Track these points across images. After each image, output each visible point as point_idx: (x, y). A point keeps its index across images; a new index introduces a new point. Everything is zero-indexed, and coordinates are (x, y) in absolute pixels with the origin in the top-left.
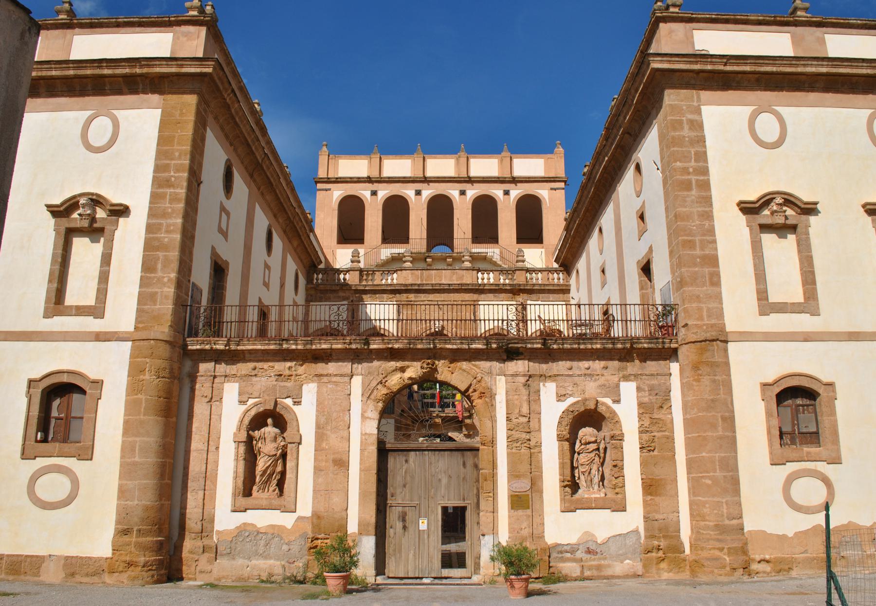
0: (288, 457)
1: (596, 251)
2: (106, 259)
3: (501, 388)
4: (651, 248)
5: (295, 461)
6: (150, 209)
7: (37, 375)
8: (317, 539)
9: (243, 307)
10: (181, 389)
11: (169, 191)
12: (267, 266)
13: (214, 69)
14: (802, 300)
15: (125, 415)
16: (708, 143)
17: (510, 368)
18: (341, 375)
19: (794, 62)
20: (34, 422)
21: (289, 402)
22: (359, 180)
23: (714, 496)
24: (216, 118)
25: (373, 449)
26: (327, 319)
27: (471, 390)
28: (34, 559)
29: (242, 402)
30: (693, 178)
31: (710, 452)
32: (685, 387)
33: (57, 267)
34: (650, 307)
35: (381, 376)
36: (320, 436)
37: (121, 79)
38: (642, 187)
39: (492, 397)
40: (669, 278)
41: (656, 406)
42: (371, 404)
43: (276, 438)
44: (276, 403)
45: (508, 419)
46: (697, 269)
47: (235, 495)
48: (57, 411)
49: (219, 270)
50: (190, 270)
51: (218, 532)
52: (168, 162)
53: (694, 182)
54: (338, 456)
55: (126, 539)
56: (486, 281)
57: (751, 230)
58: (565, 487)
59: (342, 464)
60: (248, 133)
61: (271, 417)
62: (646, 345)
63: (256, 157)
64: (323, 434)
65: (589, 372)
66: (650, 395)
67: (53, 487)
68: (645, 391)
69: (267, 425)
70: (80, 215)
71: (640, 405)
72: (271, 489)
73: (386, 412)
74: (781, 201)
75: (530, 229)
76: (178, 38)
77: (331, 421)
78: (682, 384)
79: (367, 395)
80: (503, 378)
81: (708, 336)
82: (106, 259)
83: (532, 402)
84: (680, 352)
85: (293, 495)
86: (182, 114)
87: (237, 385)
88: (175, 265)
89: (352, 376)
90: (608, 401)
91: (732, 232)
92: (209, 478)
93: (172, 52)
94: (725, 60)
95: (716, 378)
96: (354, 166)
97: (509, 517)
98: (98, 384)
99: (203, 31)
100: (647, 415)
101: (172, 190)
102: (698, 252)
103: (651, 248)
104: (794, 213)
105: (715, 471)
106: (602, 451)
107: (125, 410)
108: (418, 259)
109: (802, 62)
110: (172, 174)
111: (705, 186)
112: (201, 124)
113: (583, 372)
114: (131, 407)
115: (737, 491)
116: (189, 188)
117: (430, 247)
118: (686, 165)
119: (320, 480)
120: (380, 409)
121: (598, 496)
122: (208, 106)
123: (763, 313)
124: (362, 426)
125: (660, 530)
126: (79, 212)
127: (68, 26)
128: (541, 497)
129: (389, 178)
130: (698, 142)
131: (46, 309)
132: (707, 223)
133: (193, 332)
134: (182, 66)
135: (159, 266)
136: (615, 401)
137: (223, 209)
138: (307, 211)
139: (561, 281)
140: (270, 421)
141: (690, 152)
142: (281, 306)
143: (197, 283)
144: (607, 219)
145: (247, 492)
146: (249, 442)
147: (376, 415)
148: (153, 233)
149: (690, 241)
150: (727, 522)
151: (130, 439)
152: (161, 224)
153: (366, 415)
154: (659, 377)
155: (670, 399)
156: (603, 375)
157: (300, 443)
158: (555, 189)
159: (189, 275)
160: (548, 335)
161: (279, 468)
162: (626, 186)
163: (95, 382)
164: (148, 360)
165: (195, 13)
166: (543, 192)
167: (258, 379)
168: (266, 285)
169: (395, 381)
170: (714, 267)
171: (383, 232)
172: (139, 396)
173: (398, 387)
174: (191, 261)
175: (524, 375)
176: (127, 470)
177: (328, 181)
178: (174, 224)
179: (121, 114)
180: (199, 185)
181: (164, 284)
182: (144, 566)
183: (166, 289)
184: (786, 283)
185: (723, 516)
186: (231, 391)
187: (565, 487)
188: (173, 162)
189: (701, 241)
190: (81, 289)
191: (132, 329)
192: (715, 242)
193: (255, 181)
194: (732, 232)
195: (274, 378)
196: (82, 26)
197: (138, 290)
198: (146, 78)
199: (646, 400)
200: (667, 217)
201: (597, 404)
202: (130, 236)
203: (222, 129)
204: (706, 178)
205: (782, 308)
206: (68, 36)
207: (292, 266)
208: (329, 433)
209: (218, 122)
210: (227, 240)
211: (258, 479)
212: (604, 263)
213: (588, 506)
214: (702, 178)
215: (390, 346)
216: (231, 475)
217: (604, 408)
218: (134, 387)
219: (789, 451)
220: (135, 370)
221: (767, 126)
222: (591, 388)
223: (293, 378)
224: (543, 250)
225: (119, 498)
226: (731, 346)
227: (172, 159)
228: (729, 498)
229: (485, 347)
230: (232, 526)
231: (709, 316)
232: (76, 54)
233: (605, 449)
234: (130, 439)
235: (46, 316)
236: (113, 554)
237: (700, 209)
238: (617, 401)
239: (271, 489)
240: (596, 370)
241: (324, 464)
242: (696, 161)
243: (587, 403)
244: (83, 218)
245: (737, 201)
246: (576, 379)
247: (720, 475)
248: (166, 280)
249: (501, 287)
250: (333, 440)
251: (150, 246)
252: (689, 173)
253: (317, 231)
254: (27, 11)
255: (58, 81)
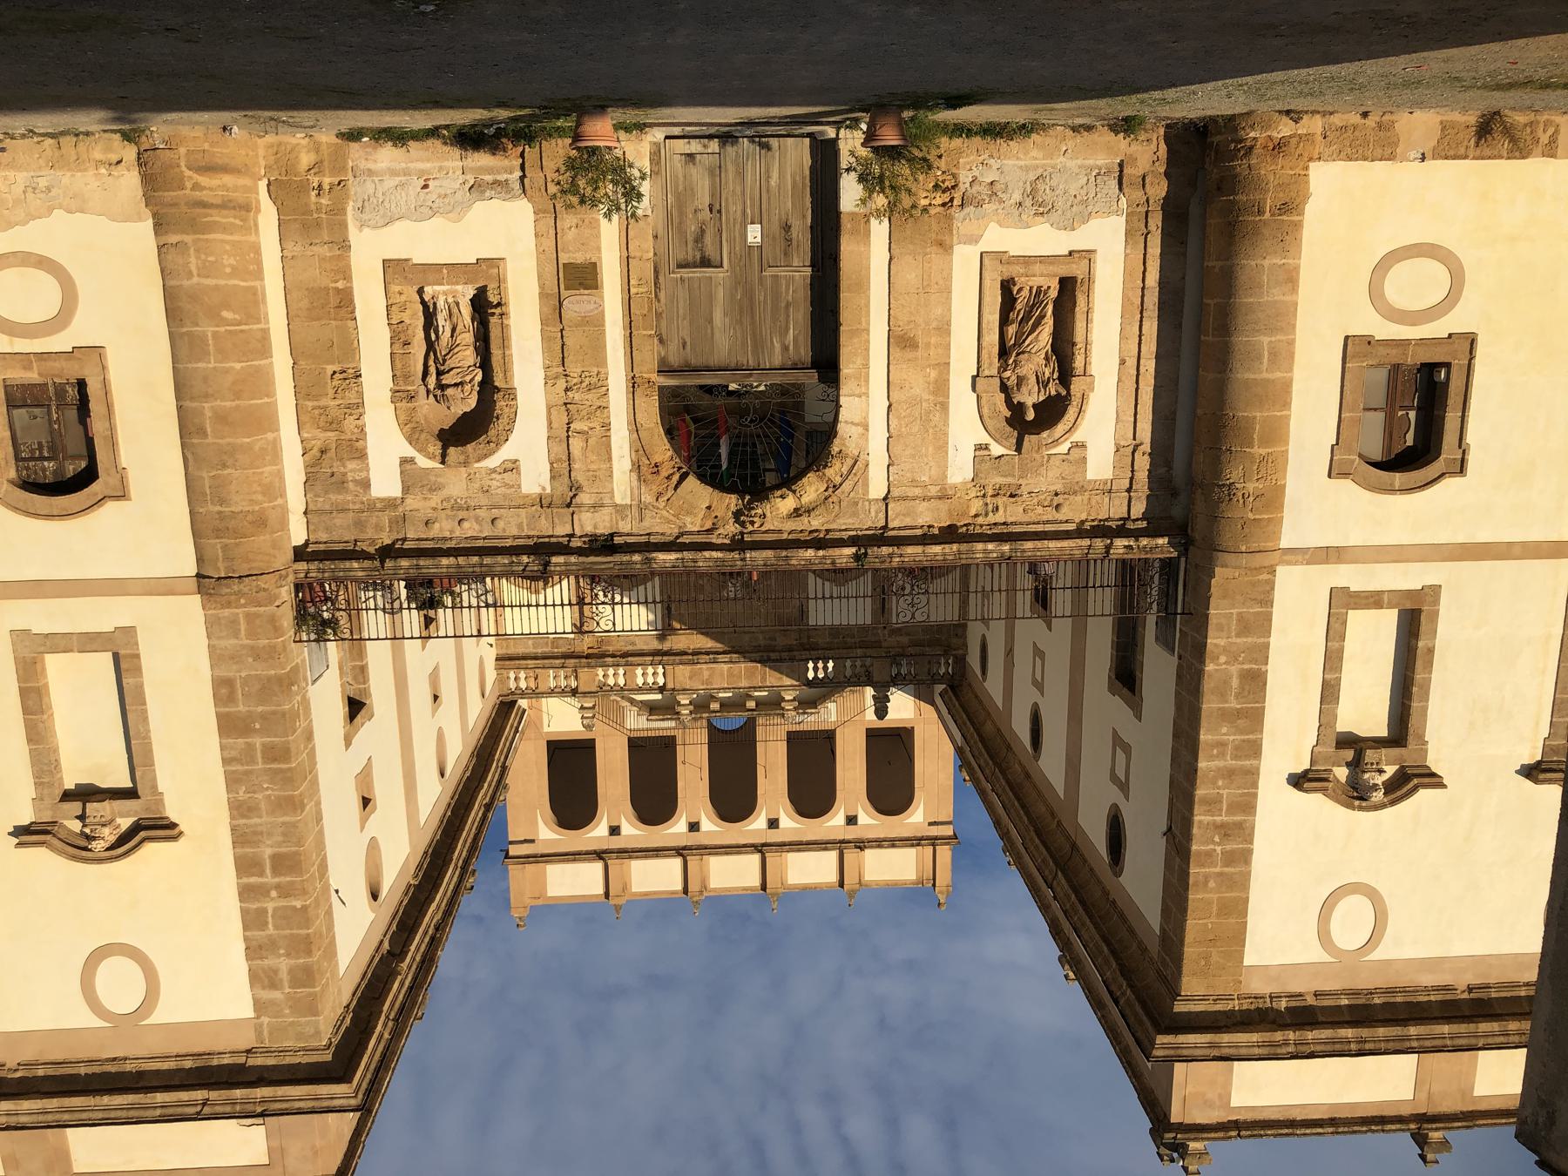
0: (996, 350)
1: (453, 731)
2: (1330, 693)
3: (622, 482)
4: (348, 742)
5: (984, 344)
6: (1255, 785)
7: (1449, 483)
8: (944, 205)
9: (1080, 616)
10: (1190, 464)
11: (1223, 818)
12: (1039, 686)
13: (1153, 1043)
14: (49, 658)
15: (1288, 417)
16: (241, 946)
17: (607, 518)
18: (905, 498)
19: (66, 1117)
20: (1454, 398)
21: (997, 450)
22: (879, 843)
23: (217, 288)
24: (1144, 950)
25: (846, 370)
26: (933, 597)
27: (676, 477)
28: (1452, 153)
29: (1082, 446)
30: (269, 879)
31: (227, 371)
32: (275, 490)
33: (1418, 677)
34: (347, 636)
35: (834, 498)
36: (941, 388)
37: (1321, 1019)
38: (367, 848)
39: (637, 467)
40: (313, 691)
41: (332, 453)
42: (852, 450)
43: (1019, 385)
44: (1019, 449)
45: (606, 426)
46: (260, 709)
47: (1090, 279)
48: (1416, 416)
49: (1126, 677)
50: (1179, 676)
51: (1117, 213)
52: (1226, 870)
53: (268, 871)
54: (910, 354)
55: (1282, 197)
56: (650, 670)
57: (155, 787)
58: (499, 304)
59: (900, 341)
60: (1083, 924)
61: (1034, 418)
62: (355, 565)
63: (1069, 881)
64: (935, 393)
65: (461, 514)
66: (344, 474)
67: (1416, 285)
68: (355, 481)
69: (1034, 406)
70: (1381, 771)
71: (362, 455)
72: (1025, 293)
73: (826, 433)
74: (94, 844)
75: (571, 767)
76: (1220, 1096)
77: (920, 418)
78: (283, 494)
79: (857, 465)
80: (618, 500)
81: (236, 586)
82: (1330, 693)
83: (565, 457)
84: (291, 555)
85: (987, 283)
86: (1207, 957)
87: (1090, 476)
88: (1208, 685)
89: (885, 499)
90: (423, 462)
91: (192, 777)
92: (1134, 310)
93: (1231, 1071)
94: (207, 1110)
95: (218, 508)
96: (892, 867)
97: (599, 249)
98: (1335, 471)
99: (1175, 1117)
100: (349, 436)
101: (1218, 819)
102: (258, 741)
103: (348, 742)
104: (66, 823)
105: (215, 334)
106: (432, 370)
107: (1288, 425)
108: (773, 704)
109: (50, 1117)
110: (1219, 849)
111: (245, 866)
112: (1172, 940)
113: (472, 513)
114: (1277, 433)
115: (170, 296)
116: (1187, 823)
117: (751, 725)
118: (283, 903)
119: (939, 311)
120: (836, 441)
121: (437, 288)
122: (1158, 972)
123: (129, 632)
124: (866, 410)
125: (318, 224)
126: (1385, 777)
127: (1423, 1119)
128: (542, 287)
129: (826, 849)
130: (260, 947)
131: (1436, 601)
132: (242, 794)
133: (1168, 566)
134: (1212, 1045)
135: (1235, 683)
136: (411, 460)
137: (1124, 787)
138: (969, 784)
139: (512, 675)
140: (1030, 415)
141: (276, 927)
142: (1011, 618)
143: (1165, 654)
144: (433, 795)
145: (1068, 286)
146: (1065, 374)
147: (841, 427)
148: (1248, 741)
149: (275, 760)
150: (188, 238)
151: (1279, 374)
152: (1235, 757)
153: (860, 430)
154: (327, 507)
155: (306, 467)
156: (434, 509)
157: (974, 378)
158: (526, 841)
159: (1179, 666)
160: (533, 579)
161: (1012, 330)
162: (399, 859)
163: (1344, 475)
164: (1251, 516)
165: (1193, 1145)
166: (548, 834)
167: (1053, 488)
168: (1039, 653)
169: (811, 488)
170: (228, 715)
171: (833, 752)
172: (1263, 451)
173: (805, 480)
174: (1177, 694)
175: (579, 506)
176: (1284, 319)
177: (933, 841)
178: (1211, 758)
179: (1317, 954)
180: (1170, 829)
181: (1225, 650)
182: (1251, 148)
183: (1222, 642)
184: (82, 689)
185: (197, 251)
186: (1101, 464)
187: (499, 304)
188: (1218, 870)
189: (253, 761)
190: (1373, 637)
191: (1280, 570)
192: (225, 761)
193: (1068, 837)
194: (192, 777)
195: (1024, 490)
196: (1399, 1119)
197: (1272, 640)
198: (1274, 1022)
199: (351, 465)
200: (318, 803)
201: (444, 456)
202: (1288, 737)
203: (1132, 931)
204: (245, 880)
205: (88, 642)
206: (1423, 1096)
207: (993, 686)
208: (926, 396)
209: (1140, 943)
210: (1114, 731)
211: (1050, 308)
212: (434, 711)
213: (456, 271)
214: (253, 880)
215: (821, 553)
216: (1096, 316)
217: (431, 449)
218: (1274, 465)
219: (72, 371)
220: (1273, 499)
221: (120, 988)
222: (456, 483)
223: (990, 492)
224: (546, 729)
225: (1297, 269)
226: (192, 570)
227: (1221, 874)
228: (186, 283)
229: (654, 555)
230: (1094, 223)
231: (234, 622)
232: (1406, 1064)
233: (425, 374)
234: (1279, 374)
235: (1435, 590)
236: (1307, 168)
237: (256, 820)
238: (405, 461)
239: (1025, 293)
240: (448, 517)
241: (933, 340)
242: (265, 911)
243: (462, 458)
244: (1377, 767)
245: (182, 840)
246: (484, 501)
247: (194, 319)
248: (1223, 659)
249: (622, 661)
250: (916, 383)
251: (1254, 718)
252: (278, 887)
253: (949, 749)
254: (1542, 1164)
255: (1437, 1014)
